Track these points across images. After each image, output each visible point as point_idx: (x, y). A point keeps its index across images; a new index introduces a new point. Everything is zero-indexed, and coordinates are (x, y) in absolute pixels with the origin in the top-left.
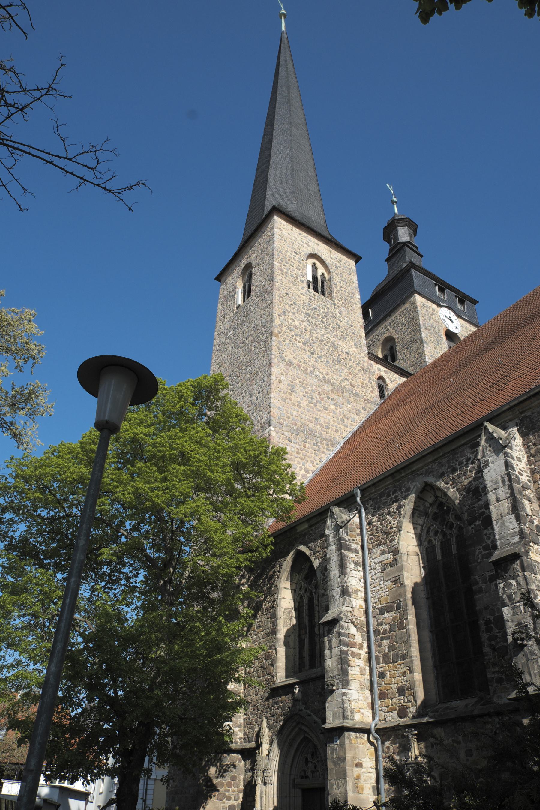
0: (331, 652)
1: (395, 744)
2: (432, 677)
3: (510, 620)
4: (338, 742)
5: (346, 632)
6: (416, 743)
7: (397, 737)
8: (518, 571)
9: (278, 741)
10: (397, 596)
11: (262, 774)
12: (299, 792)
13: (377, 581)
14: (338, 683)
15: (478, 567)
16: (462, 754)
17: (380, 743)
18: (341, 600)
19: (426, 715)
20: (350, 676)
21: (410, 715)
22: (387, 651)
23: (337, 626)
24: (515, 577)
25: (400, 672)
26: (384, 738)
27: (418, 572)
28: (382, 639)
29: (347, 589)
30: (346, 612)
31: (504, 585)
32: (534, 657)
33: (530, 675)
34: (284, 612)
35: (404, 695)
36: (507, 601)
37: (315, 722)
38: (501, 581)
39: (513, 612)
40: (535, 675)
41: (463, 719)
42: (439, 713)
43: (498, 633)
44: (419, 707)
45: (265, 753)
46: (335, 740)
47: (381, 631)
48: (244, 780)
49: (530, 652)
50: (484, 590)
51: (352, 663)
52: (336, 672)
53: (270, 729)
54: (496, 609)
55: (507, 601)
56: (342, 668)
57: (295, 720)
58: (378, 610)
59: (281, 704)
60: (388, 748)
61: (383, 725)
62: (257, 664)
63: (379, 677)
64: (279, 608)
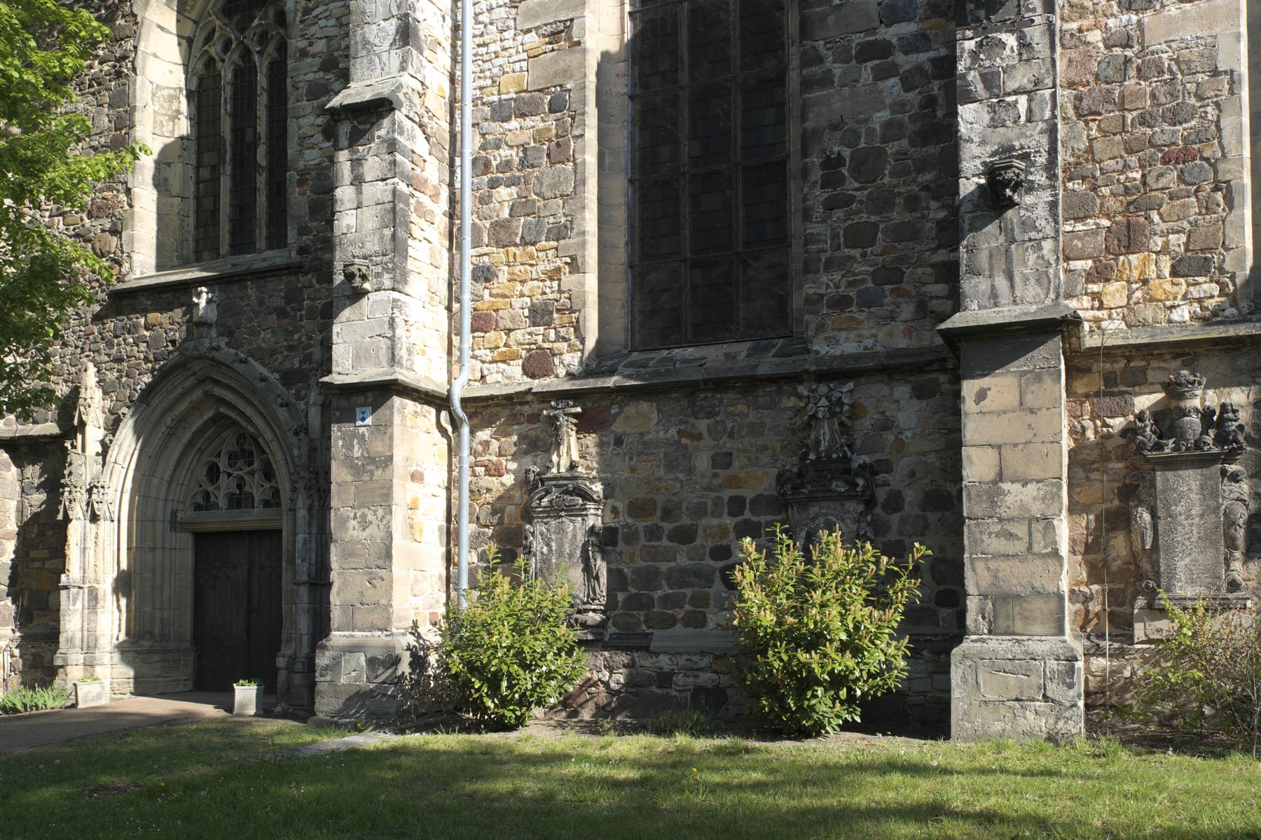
0: (359, 192)
1: (507, 435)
2: (620, 290)
3: (976, 139)
4: (369, 421)
5: (407, 143)
6: (573, 433)
7: (514, 419)
8: (1034, 10)
9: (136, 423)
10: (556, 74)
11: (86, 496)
12: (187, 540)
13: (492, 28)
14: (378, 275)
15: (831, 19)
16: (702, 462)
17: (465, 430)
18: (394, 58)
19: (612, 372)
20: (410, 260)
21: (562, 372)
22: (505, 214)
23: (386, 122)
24: (1018, 26)
25: (541, 267)
26: (475, 421)
27: (614, 26)
28: (494, 184)
29: (416, 30)
30: (410, 92)
31: (980, 45)
32: (1033, 235)
33: (1010, 278)
34: (153, 95)
35: (548, 325)
36: (979, 88)
37: (263, 379)
38: (969, 33)
39: (992, 119)
40: (1026, 279)
41: (719, 384)
42: (648, 370)
43: (857, 190)
44: (590, 354)
45: (93, 447)
46: (359, 415)
47: (494, 163)
48: (20, 511)
49: (1023, 223)
50: (836, 79)
51: (415, 231)
52: (372, 246)
53: (105, 393)
54: (863, 131)
55: (979, 88)
56: (394, 236)
57: (194, 374)
58: (487, 109)
59: (147, 334)
60: (486, 444)
61: (480, 391)
62: (61, 226)
63: (475, 278)
64: (139, 78)
